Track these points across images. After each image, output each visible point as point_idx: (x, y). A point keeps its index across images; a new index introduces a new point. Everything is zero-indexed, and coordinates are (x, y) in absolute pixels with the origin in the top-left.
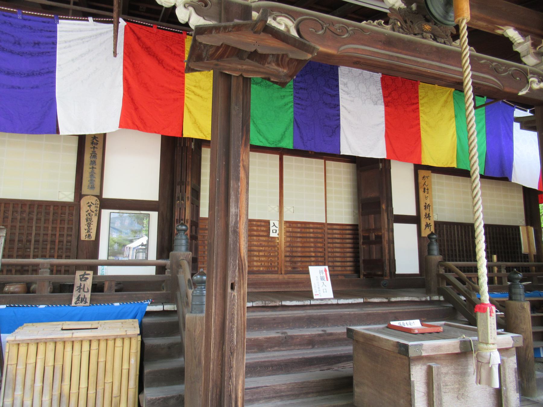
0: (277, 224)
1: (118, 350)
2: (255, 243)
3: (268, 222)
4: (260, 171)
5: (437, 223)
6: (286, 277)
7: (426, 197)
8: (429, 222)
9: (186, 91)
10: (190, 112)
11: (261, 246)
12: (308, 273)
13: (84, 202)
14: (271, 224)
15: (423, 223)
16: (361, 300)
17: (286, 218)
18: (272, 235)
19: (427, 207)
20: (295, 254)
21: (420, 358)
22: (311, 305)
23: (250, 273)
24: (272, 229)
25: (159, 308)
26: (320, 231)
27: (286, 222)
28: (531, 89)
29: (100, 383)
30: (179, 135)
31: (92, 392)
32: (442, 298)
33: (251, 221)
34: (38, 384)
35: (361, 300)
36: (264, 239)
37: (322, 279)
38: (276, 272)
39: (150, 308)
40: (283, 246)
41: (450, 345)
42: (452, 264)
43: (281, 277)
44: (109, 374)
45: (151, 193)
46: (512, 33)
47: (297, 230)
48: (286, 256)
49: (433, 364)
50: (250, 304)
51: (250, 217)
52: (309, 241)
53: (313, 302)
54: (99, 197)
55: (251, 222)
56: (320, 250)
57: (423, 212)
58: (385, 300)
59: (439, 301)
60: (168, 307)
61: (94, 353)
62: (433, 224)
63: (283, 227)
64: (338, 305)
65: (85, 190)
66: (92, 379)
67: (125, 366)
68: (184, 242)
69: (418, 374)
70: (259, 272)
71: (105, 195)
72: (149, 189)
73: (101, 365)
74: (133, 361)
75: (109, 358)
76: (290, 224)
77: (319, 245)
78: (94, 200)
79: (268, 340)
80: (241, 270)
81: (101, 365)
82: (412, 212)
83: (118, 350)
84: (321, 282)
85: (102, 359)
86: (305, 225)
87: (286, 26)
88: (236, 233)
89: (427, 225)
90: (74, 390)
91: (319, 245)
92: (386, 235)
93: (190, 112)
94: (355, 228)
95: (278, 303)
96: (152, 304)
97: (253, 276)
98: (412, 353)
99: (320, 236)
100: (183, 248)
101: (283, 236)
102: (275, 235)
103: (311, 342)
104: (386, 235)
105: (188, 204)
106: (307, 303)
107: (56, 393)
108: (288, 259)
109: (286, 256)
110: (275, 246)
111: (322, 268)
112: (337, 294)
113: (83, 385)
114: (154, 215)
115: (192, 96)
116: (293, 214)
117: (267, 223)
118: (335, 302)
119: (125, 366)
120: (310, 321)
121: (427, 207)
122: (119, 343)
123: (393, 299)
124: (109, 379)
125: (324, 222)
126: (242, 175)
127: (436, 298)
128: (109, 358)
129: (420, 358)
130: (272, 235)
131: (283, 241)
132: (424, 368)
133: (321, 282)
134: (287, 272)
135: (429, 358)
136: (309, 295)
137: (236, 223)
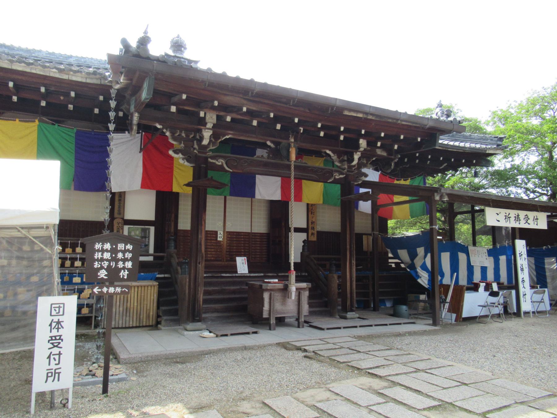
0: (222, 233)
1: (149, 291)
2: (209, 244)
3: (216, 232)
4: (214, 204)
5: (318, 232)
6: (226, 263)
7: (313, 217)
8: (313, 232)
9: (174, 168)
10: (176, 178)
11: (212, 245)
12: (235, 261)
13: (115, 222)
14: (219, 233)
15: (310, 232)
16: (262, 274)
17: (227, 230)
18: (219, 239)
19: (313, 223)
20: (232, 250)
21: (267, 290)
22: (236, 276)
23: (205, 261)
24: (219, 236)
25: (162, 276)
26: (247, 237)
27: (227, 232)
28: (335, 178)
29: (142, 304)
30: (170, 191)
31: (139, 307)
32: (306, 274)
33: (207, 231)
34: (118, 303)
35: (262, 274)
36: (214, 241)
37: (243, 263)
38: (220, 261)
39: (158, 276)
40: (225, 246)
41: (280, 286)
42: (312, 256)
43: (223, 263)
44: (145, 301)
45: (151, 216)
46: (328, 152)
47: (232, 236)
48: (227, 252)
49: (272, 292)
50: (205, 275)
51: (206, 229)
52: (240, 242)
53: (237, 275)
54: (123, 219)
55: (207, 232)
56: (247, 248)
57: (310, 226)
58: (275, 275)
59: (305, 276)
60: (166, 276)
61: (139, 292)
62: (316, 233)
63: (226, 235)
64: (250, 276)
65: (116, 215)
66: (139, 302)
67: (152, 298)
68: (173, 245)
69: (266, 296)
70: (211, 260)
71: (126, 218)
72: (149, 214)
73: (142, 297)
74: (155, 295)
75: (146, 294)
76: (230, 233)
77: (247, 245)
78: (120, 221)
79: (213, 290)
80: (202, 258)
81: (142, 297)
82: (305, 226)
83: (149, 291)
84: (242, 266)
85: (143, 294)
86: (238, 234)
87: (222, 162)
88: (201, 244)
89: (312, 234)
90: (132, 306)
91: (247, 245)
92: (284, 240)
93: (176, 178)
94: (268, 235)
95: (219, 275)
96: (158, 274)
97: (207, 263)
98: (263, 287)
99: (247, 240)
100: (173, 248)
101: (225, 240)
102: (221, 239)
103: (234, 292)
104: (284, 240)
105: (173, 224)
106: (234, 275)
107: (125, 307)
108: (228, 253)
109: (227, 252)
110: (220, 246)
111: (243, 258)
112: (249, 272)
113: (136, 304)
114: (152, 229)
115: (177, 170)
116: (231, 228)
117: (216, 233)
118: (249, 275)
119: (152, 298)
120: (234, 283)
121: (313, 223)
122: (149, 288)
123: (280, 274)
124: (145, 303)
125: (250, 231)
126: (203, 223)
127: (304, 274)
128: (146, 294)
129: (267, 290)
130: (219, 239)
131: (225, 243)
132: (269, 293)
133: (242, 265)
134: (227, 261)
135: (271, 290)
136: (236, 272)
137: (201, 241)
